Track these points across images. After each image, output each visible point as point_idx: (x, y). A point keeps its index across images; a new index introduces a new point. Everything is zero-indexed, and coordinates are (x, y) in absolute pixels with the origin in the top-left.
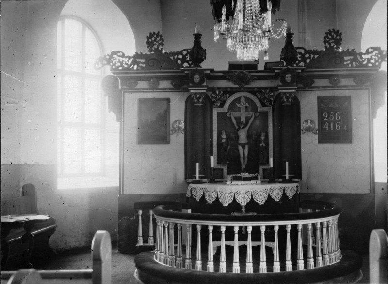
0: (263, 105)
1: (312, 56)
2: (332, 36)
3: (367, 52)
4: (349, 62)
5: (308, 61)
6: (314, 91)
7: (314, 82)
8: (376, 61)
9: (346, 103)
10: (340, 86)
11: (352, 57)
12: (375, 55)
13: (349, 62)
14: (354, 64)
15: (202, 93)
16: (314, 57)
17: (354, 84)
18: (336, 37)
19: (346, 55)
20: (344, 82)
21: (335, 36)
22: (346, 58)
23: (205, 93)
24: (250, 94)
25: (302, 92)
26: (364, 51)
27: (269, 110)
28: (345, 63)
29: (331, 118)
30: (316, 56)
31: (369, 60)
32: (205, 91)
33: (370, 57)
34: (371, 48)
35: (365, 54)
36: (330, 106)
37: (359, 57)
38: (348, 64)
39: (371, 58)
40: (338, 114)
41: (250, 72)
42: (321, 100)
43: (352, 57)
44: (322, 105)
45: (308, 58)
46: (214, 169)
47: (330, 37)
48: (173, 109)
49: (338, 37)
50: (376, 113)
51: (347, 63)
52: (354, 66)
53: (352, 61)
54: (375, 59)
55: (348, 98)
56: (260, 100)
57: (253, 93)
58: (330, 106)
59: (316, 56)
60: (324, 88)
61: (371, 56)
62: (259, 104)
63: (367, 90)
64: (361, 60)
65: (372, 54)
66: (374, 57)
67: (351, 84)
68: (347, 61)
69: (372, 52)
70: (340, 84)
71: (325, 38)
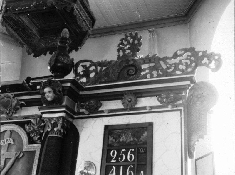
0: (31, 141)
1: (99, 68)
2: (129, 42)
3: (176, 56)
4: (147, 71)
5: (92, 75)
6: (101, 118)
7: (101, 105)
8: (187, 66)
9: (145, 134)
10: (102, 112)
11: (152, 65)
12: (187, 59)
13: (147, 71)
14: (155, 73)
15: (60, 117)
16: (101, 70)
17: (159, 104)
18: (134, 41)
19: (144, 63)
20: (144, 102)
21: (131, 40)
22: (143, 67)
23: (63, 117)
24: (17, 126)
25: (85, 120)
26: (171, 55)
27: (36, 147)
28: (142, 73)
29: (122, 159)
30: (104, 68)
31: (176, 66)
32: (62, 114)
33: (178, 62)
34: (181, 50)
35: (171, 58)
36: (121, 140)
37: (162, 63)
38: (147, 74)
39: (180, 63)
40: (131, 153)
41: (15, 96)
42: (109, 130)
43: (152, 65)
44: (111, 139)
45: (93, 71)
46: (121, 150)
47: (125, 43)
48: (126, 117)
49: (136, 42)
50: (227, 6)
51: (145, 73)
52: (155, 75)
53: (151, 69)
54: (187, 63)
55: (149, 127)
56: (28, 134)
57: (21, 124)
58: (121, 140)
59: (104, 68)
60: (112, 113)
61: (181, 61)
62: (25, 138)
63: (179, 112)
64: (165, 67)
65: (181, 58)
66: (184, 61)
67: (155, 105)
68: (144, 70)
69: (181, 55)
70: (138, 106)
71: (119, 45)
